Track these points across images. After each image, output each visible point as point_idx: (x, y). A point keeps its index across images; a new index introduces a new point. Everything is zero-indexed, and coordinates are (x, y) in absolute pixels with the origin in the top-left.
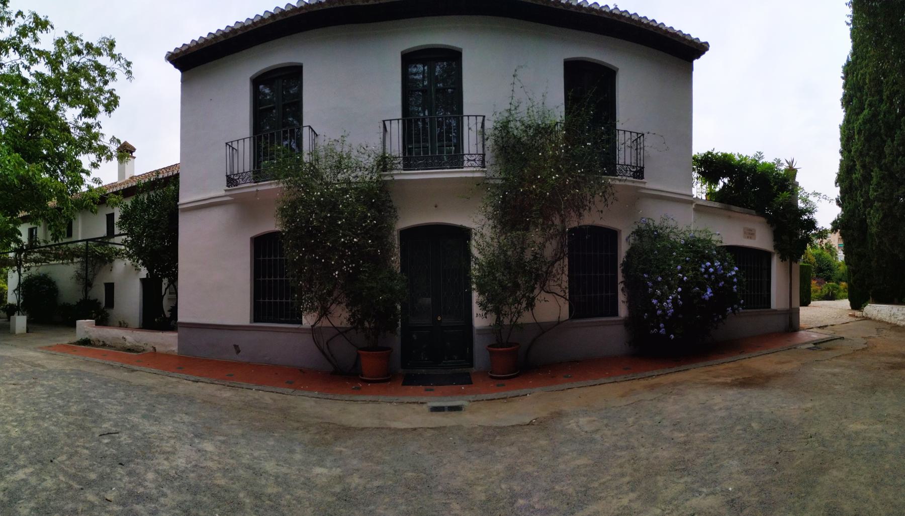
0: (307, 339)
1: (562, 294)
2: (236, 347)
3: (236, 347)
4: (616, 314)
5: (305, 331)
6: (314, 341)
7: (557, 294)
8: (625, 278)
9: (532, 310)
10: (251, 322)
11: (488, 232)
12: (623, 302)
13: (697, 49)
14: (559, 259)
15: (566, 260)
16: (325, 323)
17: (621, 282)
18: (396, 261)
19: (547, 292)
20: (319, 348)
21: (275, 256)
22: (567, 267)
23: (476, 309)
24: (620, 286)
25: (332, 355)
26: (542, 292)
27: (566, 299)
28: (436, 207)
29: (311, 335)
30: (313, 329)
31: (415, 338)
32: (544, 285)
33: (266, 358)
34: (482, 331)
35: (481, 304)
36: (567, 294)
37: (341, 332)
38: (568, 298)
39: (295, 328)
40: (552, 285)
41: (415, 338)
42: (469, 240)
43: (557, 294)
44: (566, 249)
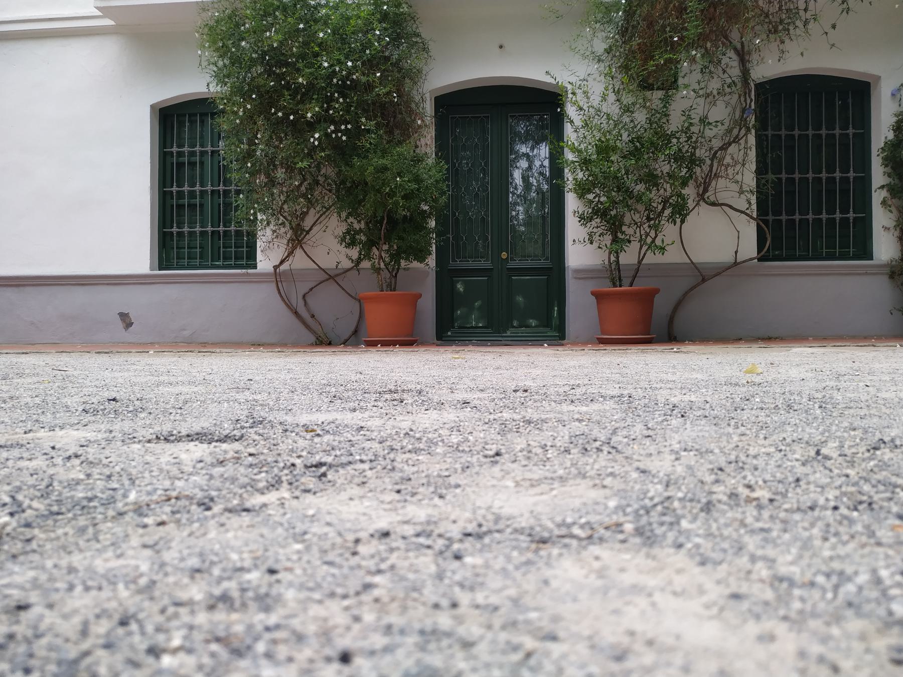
0: (269, 291)
1: (743, 206)
2: (124, 316)
3: (124, 316)
4: (864, 251)
5: (263, 278)
6: (279, 292)
7: (731, 207)
8: (889, 176)
9: (683, 222)
10: (152, 269)
11: (597, 88)
12: (886, 229)
13: (656, 291)
14: (736, 140)
15: (752, 139)
16: (299, 261)
17: (882, 187)
18: (427, 142)
19: (713, 204)
20: (289, 306)
21: (202, 146)
22: (754, 149)
23: (573, 229)
24: (878, 197)
25: (313, 316)
26: (701, 203)
27: (751, 217)
28: (501, 47)
29: (274, 285)
30: (278, 276)
31: (461, 290)
32: (706, 190)
33: (185, 333)
34: (584, 274)
35: (584, 219)
36: (754, 207)
37: (332, 277)
38: (755, 215)
39: (243, 275)
40: (724, 189)
41: (461, 290)
42: (562, 106)
43: (731, 207)
44: (752, 120)
